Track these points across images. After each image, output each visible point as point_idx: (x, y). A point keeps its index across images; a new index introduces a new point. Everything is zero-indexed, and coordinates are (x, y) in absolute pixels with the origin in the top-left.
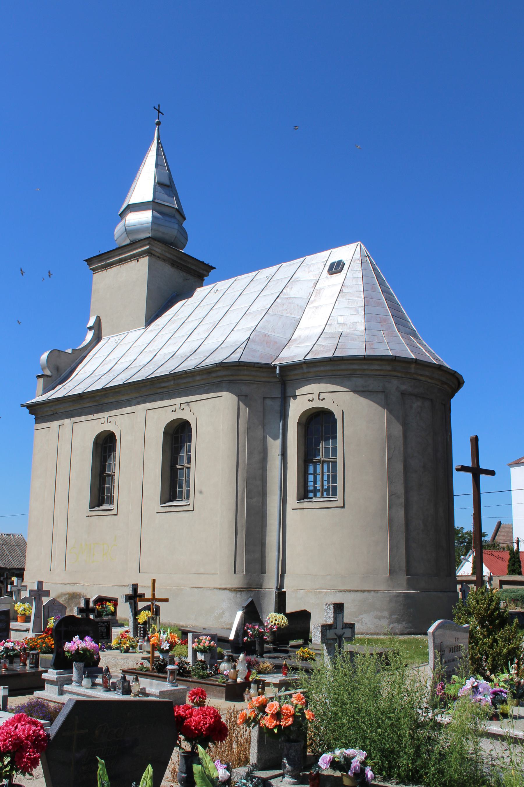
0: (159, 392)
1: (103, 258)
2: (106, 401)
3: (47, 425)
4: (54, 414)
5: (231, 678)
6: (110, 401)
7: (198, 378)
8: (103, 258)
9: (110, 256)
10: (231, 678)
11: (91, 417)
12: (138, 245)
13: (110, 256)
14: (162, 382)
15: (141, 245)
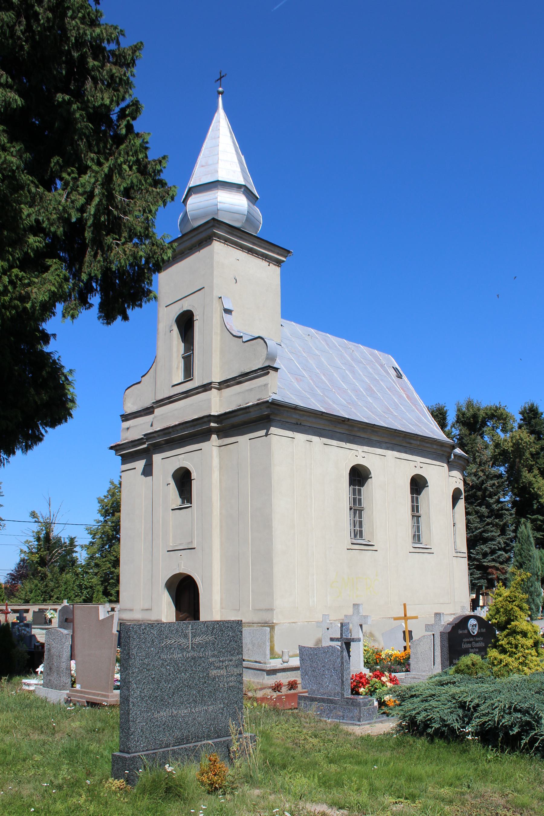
0: (403, 445)
1: (235, 233)
2: (358, 434)
3: (289, 433)
4: (297, 424)
5: (6, 617)
6: (362, 436)
7: (435, 447)
8: (235, 233)
9: (244, 237)
10: (6, 617)
11: (343, 444)
12: (277, 250)
13: (244, 237)
14: (411, 439)
15: (230, 231)
